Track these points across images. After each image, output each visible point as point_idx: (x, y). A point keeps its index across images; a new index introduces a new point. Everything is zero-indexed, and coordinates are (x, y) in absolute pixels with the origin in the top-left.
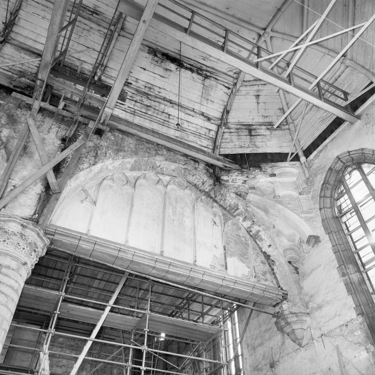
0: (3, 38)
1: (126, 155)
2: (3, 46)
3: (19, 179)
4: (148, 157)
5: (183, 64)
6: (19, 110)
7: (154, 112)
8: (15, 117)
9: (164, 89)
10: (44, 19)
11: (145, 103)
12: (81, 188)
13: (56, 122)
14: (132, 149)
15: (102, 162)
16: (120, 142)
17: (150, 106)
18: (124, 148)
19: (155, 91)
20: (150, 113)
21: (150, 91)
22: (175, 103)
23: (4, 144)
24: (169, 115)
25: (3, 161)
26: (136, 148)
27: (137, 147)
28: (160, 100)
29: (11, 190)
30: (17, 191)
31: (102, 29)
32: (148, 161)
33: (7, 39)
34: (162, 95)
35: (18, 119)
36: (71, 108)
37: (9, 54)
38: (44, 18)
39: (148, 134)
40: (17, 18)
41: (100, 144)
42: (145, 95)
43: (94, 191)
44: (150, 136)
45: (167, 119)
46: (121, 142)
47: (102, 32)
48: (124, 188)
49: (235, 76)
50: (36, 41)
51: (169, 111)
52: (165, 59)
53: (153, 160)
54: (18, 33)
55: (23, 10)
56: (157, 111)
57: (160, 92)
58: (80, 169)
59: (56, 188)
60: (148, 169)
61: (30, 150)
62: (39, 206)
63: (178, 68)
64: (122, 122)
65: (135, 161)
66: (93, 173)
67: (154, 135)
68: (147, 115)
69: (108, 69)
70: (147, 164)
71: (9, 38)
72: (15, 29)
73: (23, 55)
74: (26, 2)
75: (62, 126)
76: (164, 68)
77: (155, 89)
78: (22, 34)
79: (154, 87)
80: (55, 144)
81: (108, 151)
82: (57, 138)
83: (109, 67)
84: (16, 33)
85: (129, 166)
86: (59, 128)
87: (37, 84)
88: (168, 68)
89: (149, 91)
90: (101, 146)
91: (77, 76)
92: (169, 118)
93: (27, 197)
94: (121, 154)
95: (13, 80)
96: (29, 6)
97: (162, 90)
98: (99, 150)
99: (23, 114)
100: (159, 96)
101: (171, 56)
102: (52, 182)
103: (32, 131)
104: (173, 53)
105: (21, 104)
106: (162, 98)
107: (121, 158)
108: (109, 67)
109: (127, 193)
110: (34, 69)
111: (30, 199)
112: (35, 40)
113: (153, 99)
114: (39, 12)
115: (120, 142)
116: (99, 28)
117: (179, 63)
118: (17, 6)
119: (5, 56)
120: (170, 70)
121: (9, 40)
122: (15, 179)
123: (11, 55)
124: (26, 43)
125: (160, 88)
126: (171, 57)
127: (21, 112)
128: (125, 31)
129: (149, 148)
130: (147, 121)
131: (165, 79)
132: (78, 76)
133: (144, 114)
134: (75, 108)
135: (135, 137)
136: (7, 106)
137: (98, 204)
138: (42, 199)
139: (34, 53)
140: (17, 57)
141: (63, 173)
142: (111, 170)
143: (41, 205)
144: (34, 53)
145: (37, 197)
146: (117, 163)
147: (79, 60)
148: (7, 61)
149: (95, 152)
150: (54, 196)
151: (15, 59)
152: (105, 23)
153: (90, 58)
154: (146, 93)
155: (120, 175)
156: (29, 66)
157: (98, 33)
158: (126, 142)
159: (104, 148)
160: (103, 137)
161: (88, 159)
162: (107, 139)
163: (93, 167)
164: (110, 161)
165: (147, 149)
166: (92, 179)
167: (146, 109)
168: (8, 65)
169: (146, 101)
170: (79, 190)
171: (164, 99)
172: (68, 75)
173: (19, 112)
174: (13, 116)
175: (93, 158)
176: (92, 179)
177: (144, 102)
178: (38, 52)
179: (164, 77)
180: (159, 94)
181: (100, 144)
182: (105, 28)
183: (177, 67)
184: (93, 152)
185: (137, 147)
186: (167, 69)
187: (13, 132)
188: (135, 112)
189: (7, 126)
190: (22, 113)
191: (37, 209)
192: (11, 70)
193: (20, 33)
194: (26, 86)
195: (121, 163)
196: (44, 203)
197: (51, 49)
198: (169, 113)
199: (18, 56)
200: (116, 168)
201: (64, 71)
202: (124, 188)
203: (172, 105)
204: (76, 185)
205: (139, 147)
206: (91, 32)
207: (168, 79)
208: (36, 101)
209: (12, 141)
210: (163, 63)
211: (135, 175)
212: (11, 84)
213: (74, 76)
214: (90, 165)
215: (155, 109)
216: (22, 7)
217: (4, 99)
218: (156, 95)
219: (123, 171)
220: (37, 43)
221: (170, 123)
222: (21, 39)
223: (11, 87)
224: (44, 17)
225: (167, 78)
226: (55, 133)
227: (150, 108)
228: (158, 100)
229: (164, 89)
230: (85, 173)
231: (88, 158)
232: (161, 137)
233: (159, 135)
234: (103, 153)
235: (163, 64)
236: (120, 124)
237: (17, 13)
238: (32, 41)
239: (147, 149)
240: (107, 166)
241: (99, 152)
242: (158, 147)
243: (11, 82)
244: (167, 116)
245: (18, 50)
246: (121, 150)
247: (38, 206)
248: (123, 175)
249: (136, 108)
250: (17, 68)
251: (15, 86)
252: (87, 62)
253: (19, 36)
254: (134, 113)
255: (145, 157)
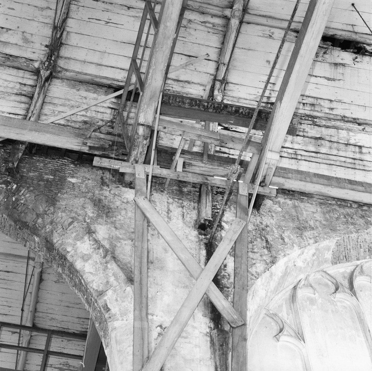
0: (49, 72)
1: (317, 235)
2: (49, 85)
3: (163, 311)
4: (357, 232)
5: (365, 47)
6: (105, 188)
7: (331, 148)
8: (106, 202)
9: (340, 101)
10: (109, 24)
11: (310, 135)
12: (264, 312)
13: (173, 198)
14: (320, 222)
15: (285, 255)
16: (294, 214)
17: (320, 138)
18: (307, 222)
19: (322, 109)
20: (323, 150)
21: (314, 111)
22: (365, 122)
23: (110, 253)
24: (360, 147)
25: (119, 283)
26: (327, 220)
27: (327, 216)
28: (338, 124)
29: (160, 334)
30: (172, 334)
31: (209, 19)
32: (359, 240)
33: (55, 72)
34: (337, 113)
35: (111, 204)
36: (194, 168)
37: (61, 97)
38: (109, 22)
39: (345, 188)
40: (65, 33)
41: (264, 223)
42: (308, 120)
43: (288, 315)
44: (346, 191)
45: (358, 156)
46: (297, 213)
47: (209, 23)
48: (335, 300)
49: (225, 97)
50: (100, 65)
51: (357, 141)
52: (331, 47)
53: (366, 236)
54: (69, 58)
55: (73, 18)
56: (335, 144)
57: (332, 109)
58: (253, 275)
59: (235, 317)
60: (362, 254)
61: (155, 255)
62: (217, 358)
63: (356, 58)
64: (290, 175)
65: (338, 245)
66: (276, 278)
67: (354, 187)
68: (319, 155)
69: (230, 87)
70: (359, 246)
71: (59, 69)
72: (64, 52)
73: (83, 93)
74: (76, 3)
75: (185, 203)
76: (330, 64)
77: (322, 104)
78: (77, 58)
79: (319, 101)
80: (190, 238)
81: (283, 232)
82: (187, 226)
83: (232, 83)
84: (66, 58)
85: (329, 255)
86: (183, 207)
87: (138, 134)
88: (339, 61)
89: (311, 110)
90: (267, 226)
91: (204, 106)
92: (361, 153)
93: (190, 343)
94: (308, 234)
95: (88, 137)
96: (81, 8)
97: (334, 103)
98: (268, 234)
99: (115, 195)
100: (332, 117)
101: (341, 38)
102: (224, 307)
103: (152, 220)
104: (343, 33)
105: (104, 178)
106: (339, 118)
107: (312, 241)
108: (232, 83)
109: (345, 307)
110: (106, 113)
111: (196, 346)
112: (99, 63)
113: (324, 123)
114: (99, 15)
115: (294, 214)
116: (201, 18)
117: (356, 48)
118: (64, 13)
119: (56, 101)
120: (343, 65)
121: (59, 72)
122: (155, 313)
123: (63, 97)
124: (85, 72)
125: (331, 101)
126: (340, 40)
127: (110, 191)
128: (250, 14)
129: (348, 214)
130: (322, 166)
131: (337, 82)
132: (206, 104)
133: (313, 154)
134: (203, 165)
135: (315, 199)
136: (84, 186)
137: (307, 336)
138: (217, 344)
139: (100, 85)
140: (75, 99)
141: (228, 288)
142: (301, 268)
143: (219, 356)
144: (100, 85)
145: (207, 341)
146: (310, 251)
147: (178, 81)
148: (60, 109)
149: (262, 240)
150: (237, 332)
151: (73, 102)
152: (215, 8)
153: (196, 73)
154: (308, 116)
155: (318, 276)
156: (97, 110)
157: (202, 28)
158: (304, 212)
159: (274, 229)
160: (261, 210)
161: (258, 255)
162: (269, 211)
163: (273, 267)
164: (295, 252)
165: (345, 217)
166: (276, 291)
167: (315, 145)
168: (64, 115)
169: (311, 129)
170: (262, 316)
171: (344, 119)
172: (187, 106)
173: (106, 192)
174: (100, 200)
175: (266, 251)
176: (276, 291)
177: (307, 132)
178: (109, 82)
179: (334, 80)
180: (331, 112)
181: (264, 223)
182: (213, 16)
183: (354, 56)
184: (259, 240)
185: (327, 216)
186: (336, 64)
187: (114, 229)
188: (296, 154)
189: (100, 220)
190: (112, 192)
191: (216, 363)
192: (69, 124)
193: (72, 57)
194: (111, 143)
195: (315, 251)
196: (223, 349)
197: (163, 64)
198: (359, 144)
199: (77, 97)
200: (308, 264)
201: (179, 102)
202: (335, 300)
203: (361, 127)
204: (256, 307)
205: (330, 217)
206: (190, 28)
207: (342, 82)
208: (136, 165)
209: (119, 245)
210: (327, 54)
211: (342, 270)
212: (85, 144)
213: (199, 106)
214: (268, 264)
215: (331, 141)
216: (72, 14)
217: (75, 175)
218: (326, 115)
219: (321, 267)
220: (104, 67)
221: (365, 163)
222: (75, 67)
223: (85, 149)
224: (108, 21)
225: (339, 80)
226: (180, 218)
227: (323, 142)
228: (333, 123)
229: (340, 101)
230: (263, 281)
231: (257, 253)
232: (368, 189)
233: (363, 186)
234: (277, 238)
235: (326, 56)
236: (289, 178)
237: (64, 24)
238: (94, 65)
239: (345, 217)
240: (294, 262)
241: (270, 238)
242: (362, 210)
243: (85, 141)
244: (357, 149)
245: (74, 87)
246: (305, 228)
247: (215, 357)
248: (324, 274)
249: (296, 146)
250: (78, 117)
251: (91, 148)
252: (193, 83)
253: (72, 62)
254: (295, 157)
255: (352, 233)
